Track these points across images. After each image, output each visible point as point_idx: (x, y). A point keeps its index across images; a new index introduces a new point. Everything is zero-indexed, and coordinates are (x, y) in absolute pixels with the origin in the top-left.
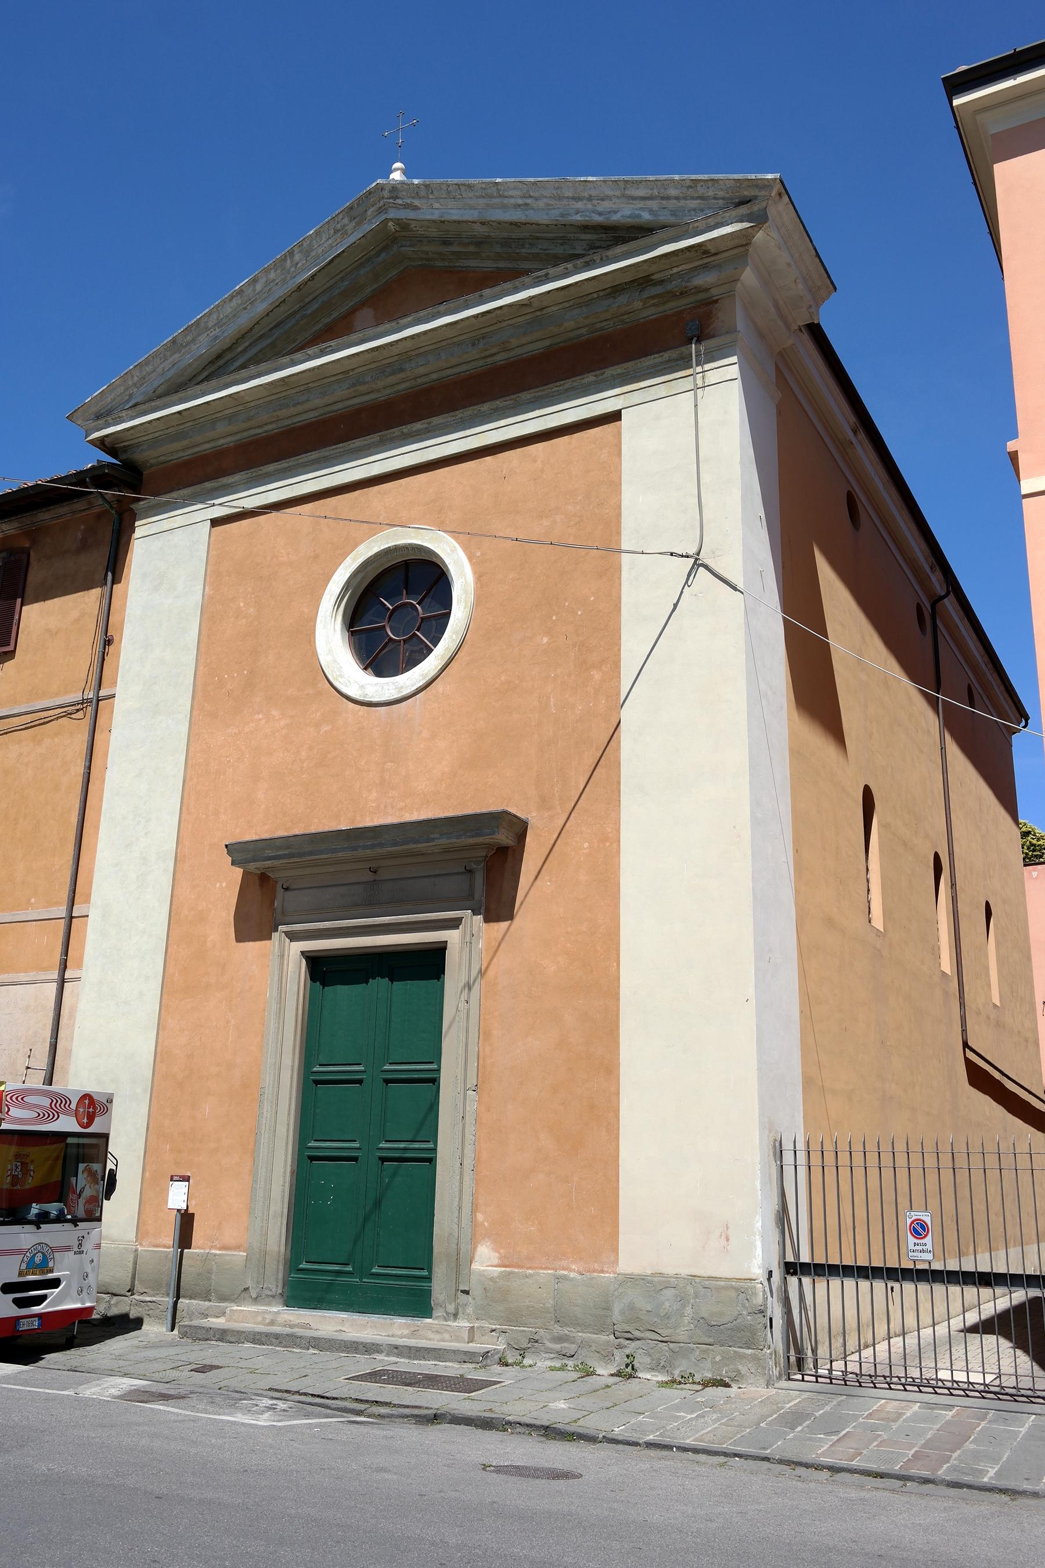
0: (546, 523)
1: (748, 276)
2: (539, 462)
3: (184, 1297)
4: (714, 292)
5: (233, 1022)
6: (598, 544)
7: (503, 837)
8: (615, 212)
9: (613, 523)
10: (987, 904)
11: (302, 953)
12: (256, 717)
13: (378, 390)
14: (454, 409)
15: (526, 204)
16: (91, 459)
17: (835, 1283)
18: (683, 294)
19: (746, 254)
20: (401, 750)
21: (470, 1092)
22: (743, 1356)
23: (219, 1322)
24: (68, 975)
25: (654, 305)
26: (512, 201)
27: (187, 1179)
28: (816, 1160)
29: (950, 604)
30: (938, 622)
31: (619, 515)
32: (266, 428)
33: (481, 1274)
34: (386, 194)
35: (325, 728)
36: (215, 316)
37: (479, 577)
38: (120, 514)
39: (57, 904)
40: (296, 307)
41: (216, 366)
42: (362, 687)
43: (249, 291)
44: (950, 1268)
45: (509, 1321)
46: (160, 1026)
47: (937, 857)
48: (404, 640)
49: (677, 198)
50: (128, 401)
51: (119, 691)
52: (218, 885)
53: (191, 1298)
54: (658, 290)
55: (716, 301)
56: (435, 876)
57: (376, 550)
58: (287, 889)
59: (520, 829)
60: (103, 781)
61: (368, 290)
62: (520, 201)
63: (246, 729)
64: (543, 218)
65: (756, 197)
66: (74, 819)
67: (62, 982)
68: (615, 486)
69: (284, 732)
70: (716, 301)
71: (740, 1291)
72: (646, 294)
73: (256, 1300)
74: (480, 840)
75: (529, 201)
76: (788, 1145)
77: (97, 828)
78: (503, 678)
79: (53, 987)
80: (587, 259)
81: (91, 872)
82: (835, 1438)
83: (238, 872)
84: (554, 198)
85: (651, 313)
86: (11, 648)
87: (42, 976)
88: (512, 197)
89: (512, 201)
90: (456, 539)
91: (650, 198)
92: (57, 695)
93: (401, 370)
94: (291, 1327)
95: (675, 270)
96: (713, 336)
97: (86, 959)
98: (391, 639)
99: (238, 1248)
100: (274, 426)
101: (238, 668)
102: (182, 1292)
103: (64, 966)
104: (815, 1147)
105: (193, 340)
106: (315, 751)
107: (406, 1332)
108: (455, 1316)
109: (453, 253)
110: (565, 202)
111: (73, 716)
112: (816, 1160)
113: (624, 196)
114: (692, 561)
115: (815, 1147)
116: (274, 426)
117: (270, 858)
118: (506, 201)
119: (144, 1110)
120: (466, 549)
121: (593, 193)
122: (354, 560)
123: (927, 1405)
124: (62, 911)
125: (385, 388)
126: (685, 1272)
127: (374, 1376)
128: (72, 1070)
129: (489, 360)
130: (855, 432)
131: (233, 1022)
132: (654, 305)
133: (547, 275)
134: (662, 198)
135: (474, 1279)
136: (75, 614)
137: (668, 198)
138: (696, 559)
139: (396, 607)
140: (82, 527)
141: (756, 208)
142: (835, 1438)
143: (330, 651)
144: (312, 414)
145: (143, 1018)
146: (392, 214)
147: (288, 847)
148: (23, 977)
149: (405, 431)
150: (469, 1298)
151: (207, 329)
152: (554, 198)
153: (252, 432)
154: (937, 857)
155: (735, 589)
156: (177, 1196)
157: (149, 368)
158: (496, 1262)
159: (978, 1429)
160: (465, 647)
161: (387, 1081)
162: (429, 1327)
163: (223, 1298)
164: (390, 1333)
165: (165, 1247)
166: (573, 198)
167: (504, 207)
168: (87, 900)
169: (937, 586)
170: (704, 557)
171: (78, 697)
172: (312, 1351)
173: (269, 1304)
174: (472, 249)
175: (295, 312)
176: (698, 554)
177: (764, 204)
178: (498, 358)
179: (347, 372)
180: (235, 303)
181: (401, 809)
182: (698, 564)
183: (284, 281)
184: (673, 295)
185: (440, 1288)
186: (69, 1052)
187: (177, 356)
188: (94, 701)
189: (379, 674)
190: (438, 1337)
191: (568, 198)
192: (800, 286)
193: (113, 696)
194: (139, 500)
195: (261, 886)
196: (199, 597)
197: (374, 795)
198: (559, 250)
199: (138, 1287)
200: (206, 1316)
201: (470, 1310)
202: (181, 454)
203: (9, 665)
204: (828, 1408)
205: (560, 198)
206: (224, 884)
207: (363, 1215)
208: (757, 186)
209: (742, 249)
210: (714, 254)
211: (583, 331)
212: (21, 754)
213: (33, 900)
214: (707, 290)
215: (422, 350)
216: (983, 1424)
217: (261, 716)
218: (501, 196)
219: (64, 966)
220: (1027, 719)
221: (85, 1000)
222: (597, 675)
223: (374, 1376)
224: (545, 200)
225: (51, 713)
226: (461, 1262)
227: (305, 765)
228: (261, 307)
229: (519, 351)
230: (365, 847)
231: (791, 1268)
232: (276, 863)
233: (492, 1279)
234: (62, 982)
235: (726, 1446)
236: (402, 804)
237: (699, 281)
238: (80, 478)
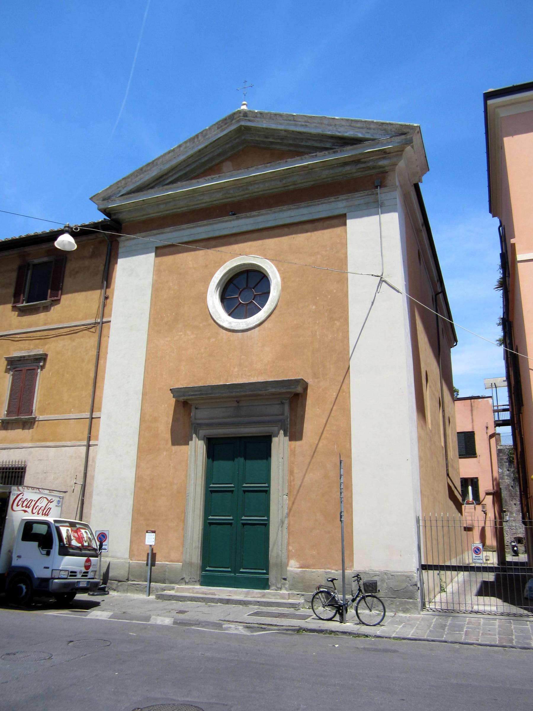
0: (313, 258)
1: (402, 164)
3: (153, 582)
4: (386, 168)
5: (172, 465)
6: (337, 268)
7: (299, 390)
8: (346, 132)
9: (343, 261)
12: (179, 334)
13: (235, 197)
14: (271, 207)
15: (306, 125)
16: (101, 217)
17: (430, 572)
18: (374, 168)
19: (401, 155)
20: (248, 351)
21: (285, 496)
22: (409, 602)
23: (172, 593)
24: (91, 443)
25: (361, 171)
26: (300, 123)
27: (154, 532)
28: (428, 524)
29: (441, 295)
31: (346, 257)
32: (182, 209)
33: (292, 571)
34: (241, 115)
35: (212, 340)
36: (161, 160)
37: (283, 279)
38: (111, 242)
39: (85, 412)
40: (197, 159)
41: (159, 181)
42: (230, 323)
43: (177, 151)
44: (447, 564)
45: (304, 590)
46: (138, 466)
48: (247, 304)
49: (374, 129)
50: (118, 194)
51: (113, 319)
52: (163, 406)
53: (156, 582)
54: (363, 166)
55: (387, 172)
56: (266, 405)
57: (235, 265)
58: (196, 408)
59: (305, 386)
60: (106, 359)
61: (229, 154)
62: (303, 124)
63: (175, 339)
64: (314, 131)
65: (408, 132)
66: (92, 375)
67: (89, 446)
69: (193, 341)
70: (387, 172)
71: (408, 577)
72: (358, 167)
73: (186, 583)
74: (289, 390)
75: (307, 124)
77: (103, 379)
78: (295, 322)
79: (84, 449)
80: (334, 150)
83: (174, 399)
84: (319, 123)
85: (359, 174)
88: (300, 121)
89: (300, 123)
90: (272, 263)
91: (362, 128)
92: (82, 319)
93: (247, 189)
94: (206, 594)
95: (371, 158)
96: (386, 186)
98: (241, 303)
99: (178, 561)
100: (186, 208)
101: (169, 313)
102: (152, 580)
103: (89, 439)
104: (427, 518)
105: (150, 169)
106: (208, 350)
107: (259, 596)
108: (281, 589)
109: (270, 142)
110: (324, 126)
111: (90, 330)
112: (428, 524)
113: (350, 126)
114: (379, 278)
116: (186, 208)
117: (192, 395)
118: (297, 123)
119: (131, 502)
120: (277, 267)
121: (337, 123)
122: (225, 268)
124: (87, 415)
125: (238, 196)
126: (383, 569)
127: (256, 614)
128: (95, 484)
129: (286, 188)
130: (422, 226)
131: (172, 465)
132: (361, 171)
133: (316, 155)
134: (367, 129)
135: (288, 574)
137: (370, 129)
138: (381, 278)
139: (244, 289)
140: (92, 247)
141: (408, 137)
143: (214, 307)
144: (204, 205)
146: (243, 123)
147: (200, 391)
148: (69, 443)
149: (248, 215)
150: (287, 582)
151: (157, 165)
152: (319, 123)
153: (175, 210)
155: (398, 292)
156: (150, 539)
157: (129, 180)
158: (298, 566)
160: (277, 308)
161: (245, 491)
162: (269, 593)
163: (172, 582)
164: (252, 596)
165: (143, 561)
166: (328, 125)
167: (296, 125)
168: (100, 410)
170: (385, 278)
171: (93, 321)
172: (219, 604)
173: (194, 585)
174: (279, 141)
175: (196, 161)
176: (382, 275)
177: (412, 136)
178: (291, 187)
179: (222, 188)
180: (170, 155)
181: (249, 376)
182: (382, 281)
183: (193, 147)
184: (369, 168)
185: (272, 576)
186: (93, 477)
187: (142, 175)
188: (101, 323)
189: (234, 317)
190: (273, 597)
191: (325, 124)
192: (418, 168)
193: (110, 322)
194: (120, 236)
195: (184, 407)
196: (150, 280)
197: (236, 369)
198: (319, 145)
199: (131, 578)
200: (165, 590)
201: (287, 586)
202: (141, 218)
205: (321, 123)
206: (166, 406)
207: (235, 546)
208: (409, 128)
209: (400, 153)
210: (389, 153)
211: (329, 179)
212: (64, 345)
213: (72, 410)
214: (384, 167)
215: (257, 182)
217: (181, 333)
218: (294, 121)
219: (89, 439)
221: (100, 454)
222: (338, 323)
223: (256, 614)
224: (315, 124)
225: (79, 328)
226: (282, 566)
227: (203, 355)
228: (182, 158)
229: (300, 185)
230: (237, 392)
231: (424, 567)
232: (193, 397)
233: (297, 573)
234: (89, 446)
236: (249, 374)
237: (382, 163)
238: (96, 225)
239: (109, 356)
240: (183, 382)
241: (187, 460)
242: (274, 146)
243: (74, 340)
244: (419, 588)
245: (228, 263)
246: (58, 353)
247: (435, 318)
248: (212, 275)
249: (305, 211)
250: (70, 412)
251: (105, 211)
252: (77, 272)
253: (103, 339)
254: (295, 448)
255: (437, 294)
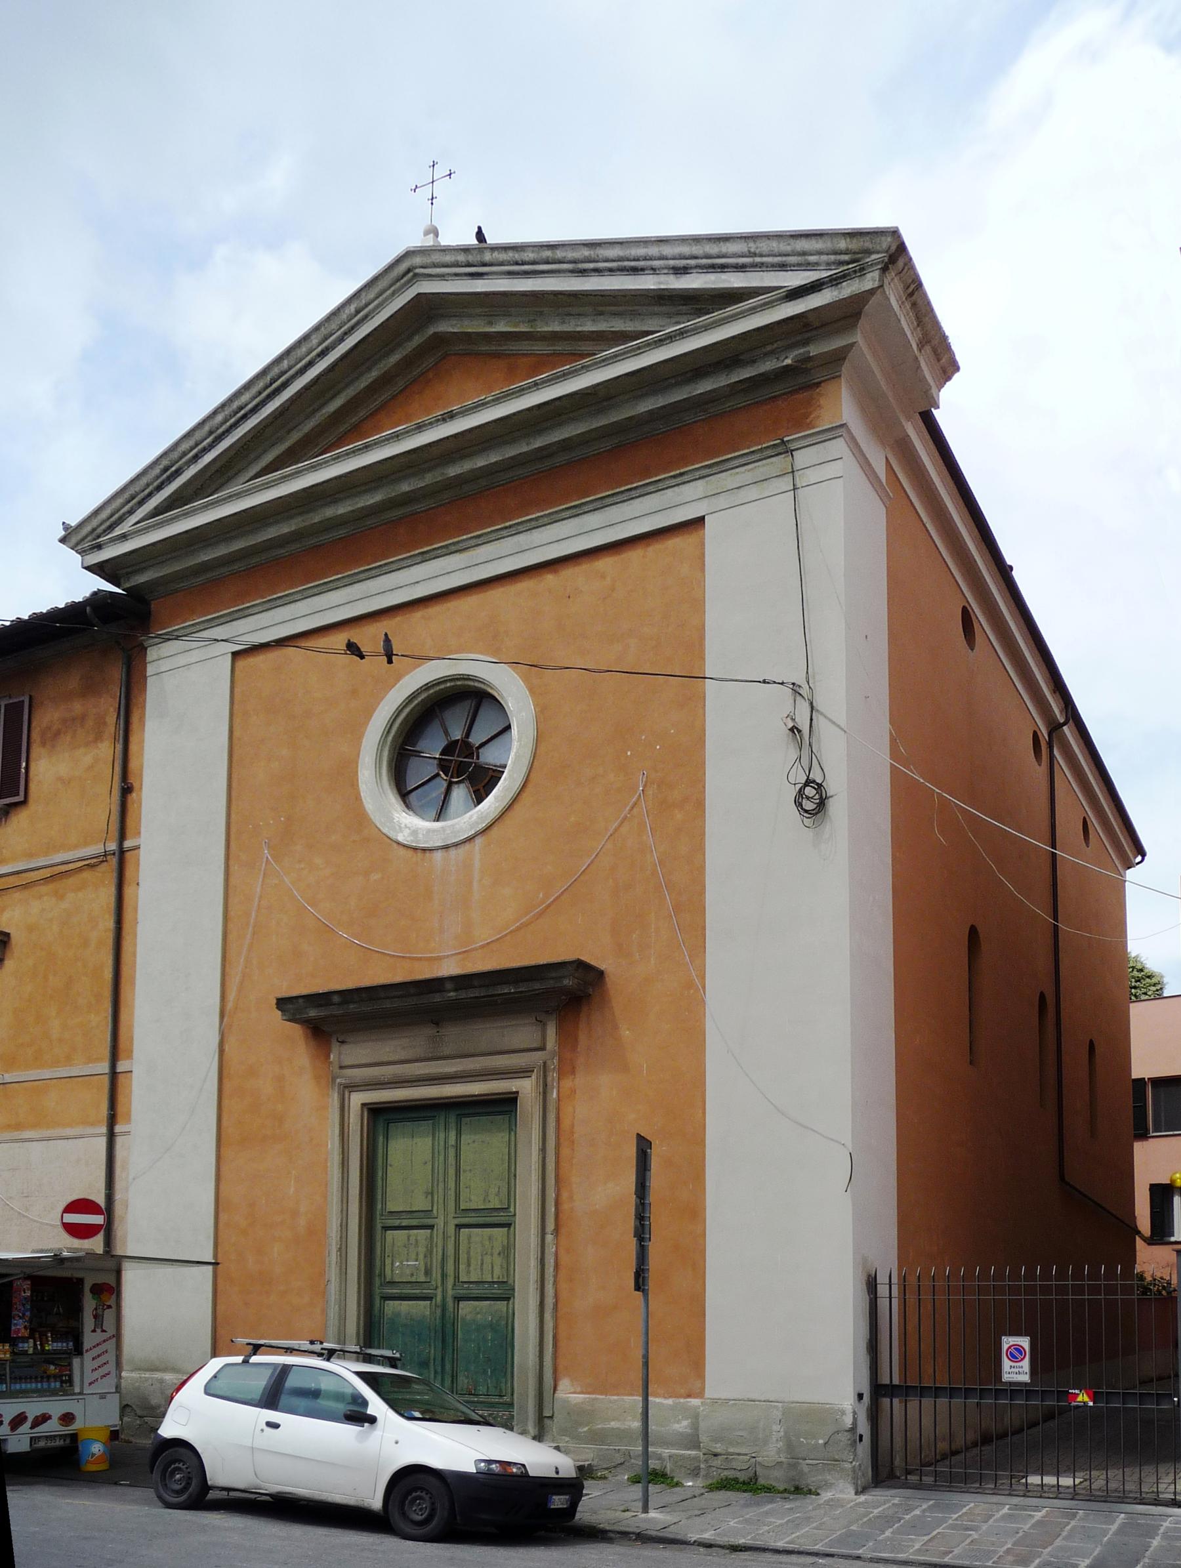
2: (609, 579)
9: (696, 646)
10: (1091, 1043)
11: (363, 1105)
24: (118, 1129)
30: (1056, 752)
31: (702, 638)
33: (566, 1401)
35: (375, 877)
39: (98, 1060)
47: (1042, 997)
66: (108, 974)
67: (111, 1137)
68: (698, 605)
76: (882, 1279)
81: (131, 1027)
82: (926, 1538)
86: (21, 798)
87: (90, 1130)
92: (76, 847)
97: (133, 1113)
115: (912, 1281)
123: (1015, 1507)
124: (105, 1067)
136: (88, 759)
142: (926, 1538)
145: (170, 1153)
154: (1042, 997)
159: (1068, 1527)
169: (1057, 711)
171: (96, 849)
193: (138, 847)
203: (20, 820)
204: (917, 1512)
212: (43, 910)
216: (1073, 1523)
220: (1143, 855)
234: (111, 1137)
235: (818, 1547)
239: (140, 928)
240: (280, 996)
241: (326, 1160)
242: (514, 347)
243: (61, 897)
244: (861, 1437)
245: (407, 679)
246: (31, 929)
247: (1049, 861)
248: (368, 713)
249: (593, 520)
250: (68, 1060)
251: (98, 569)
252: (58, 734)
253: (128, 891)
254: (573, 1126)
255: (1055, 728)
